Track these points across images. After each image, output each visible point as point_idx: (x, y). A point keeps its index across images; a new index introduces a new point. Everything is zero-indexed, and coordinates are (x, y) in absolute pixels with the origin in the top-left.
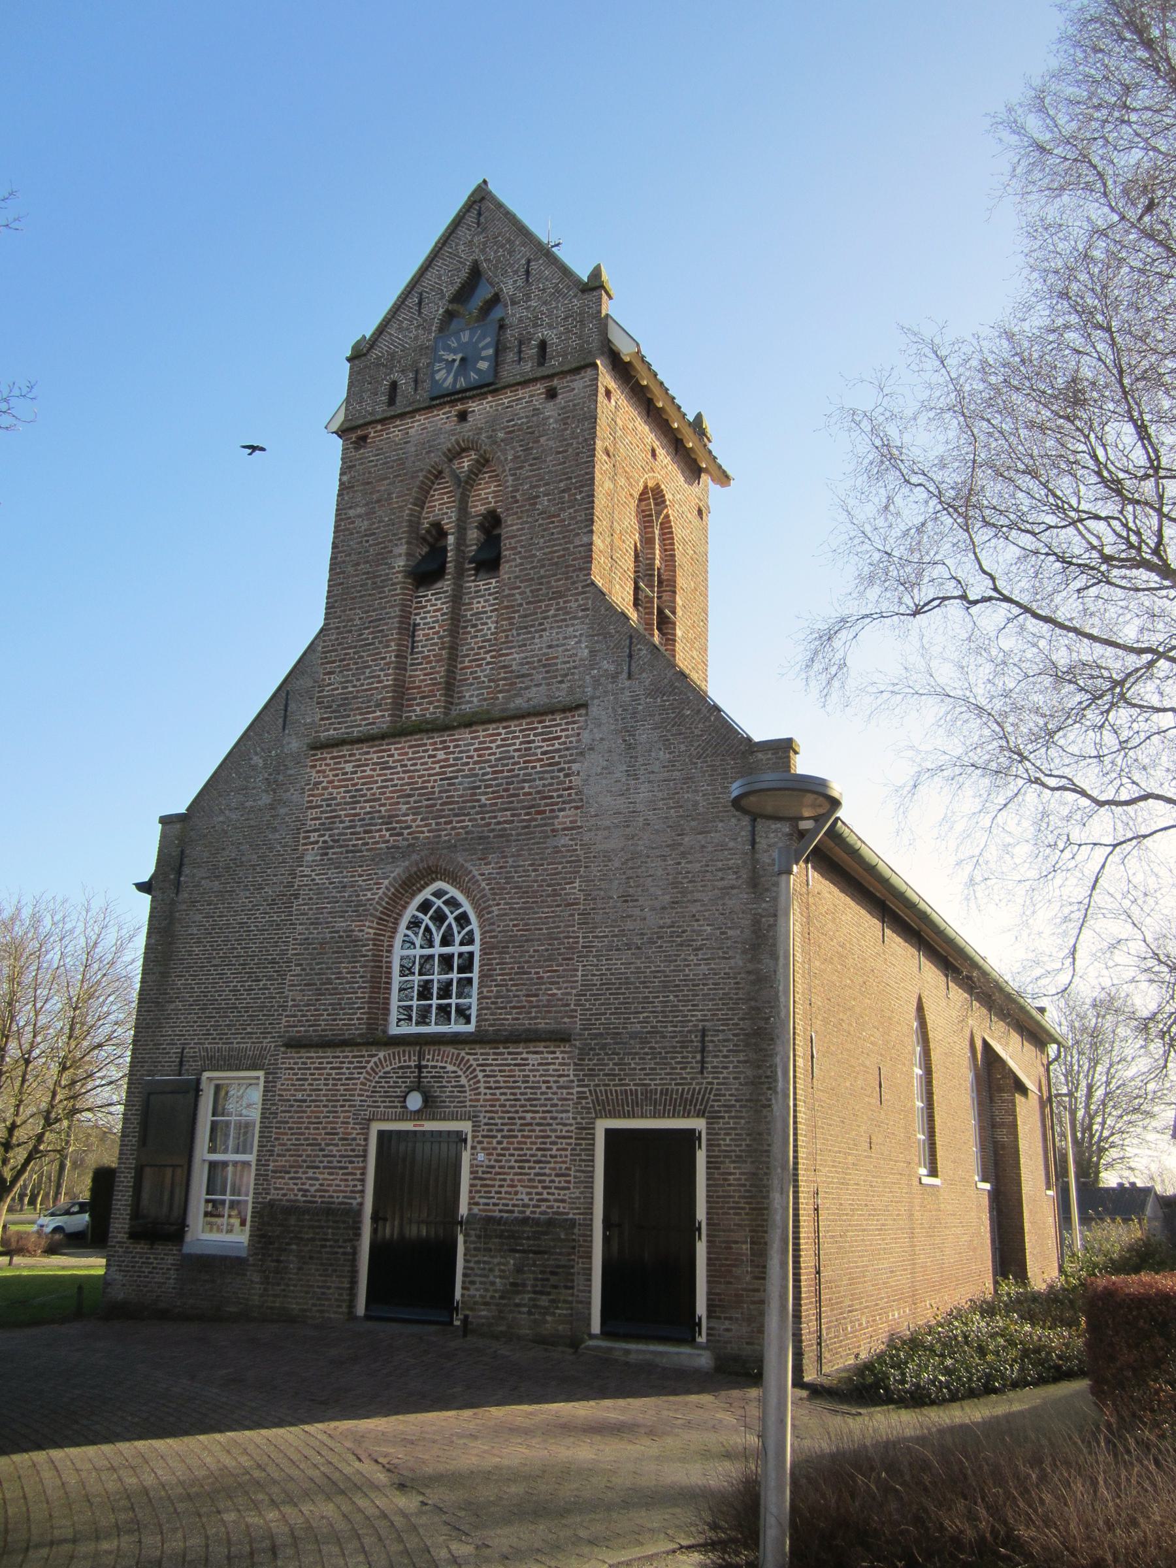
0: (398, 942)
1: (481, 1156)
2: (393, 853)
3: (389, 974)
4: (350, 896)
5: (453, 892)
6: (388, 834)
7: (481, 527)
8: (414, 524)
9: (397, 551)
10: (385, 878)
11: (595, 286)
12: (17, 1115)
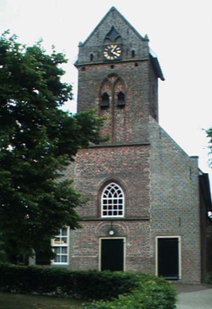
0: (102, 196)
1: (129, 244)
2: (102, 176)
3: (100, 204)
5: (116, 185)
7: (118, 96)
8: (100, 93)
9: (96, 100)
11: (146, 40)
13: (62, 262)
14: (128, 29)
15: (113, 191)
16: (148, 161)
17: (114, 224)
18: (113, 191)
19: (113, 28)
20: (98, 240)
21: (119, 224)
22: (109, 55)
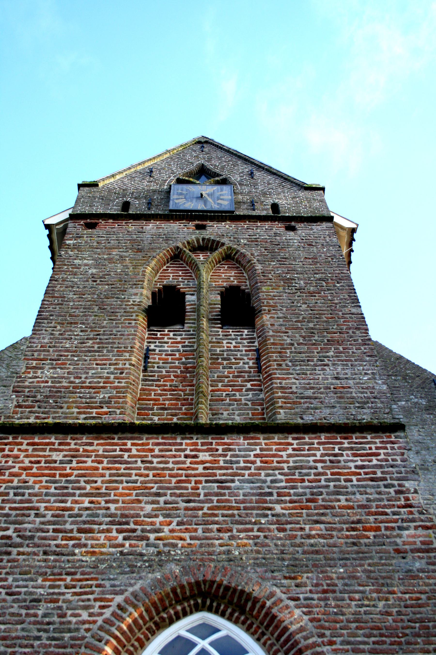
4: (45, 615)
6: (121, 537)
10: (116, 593)
12: (366, 546)
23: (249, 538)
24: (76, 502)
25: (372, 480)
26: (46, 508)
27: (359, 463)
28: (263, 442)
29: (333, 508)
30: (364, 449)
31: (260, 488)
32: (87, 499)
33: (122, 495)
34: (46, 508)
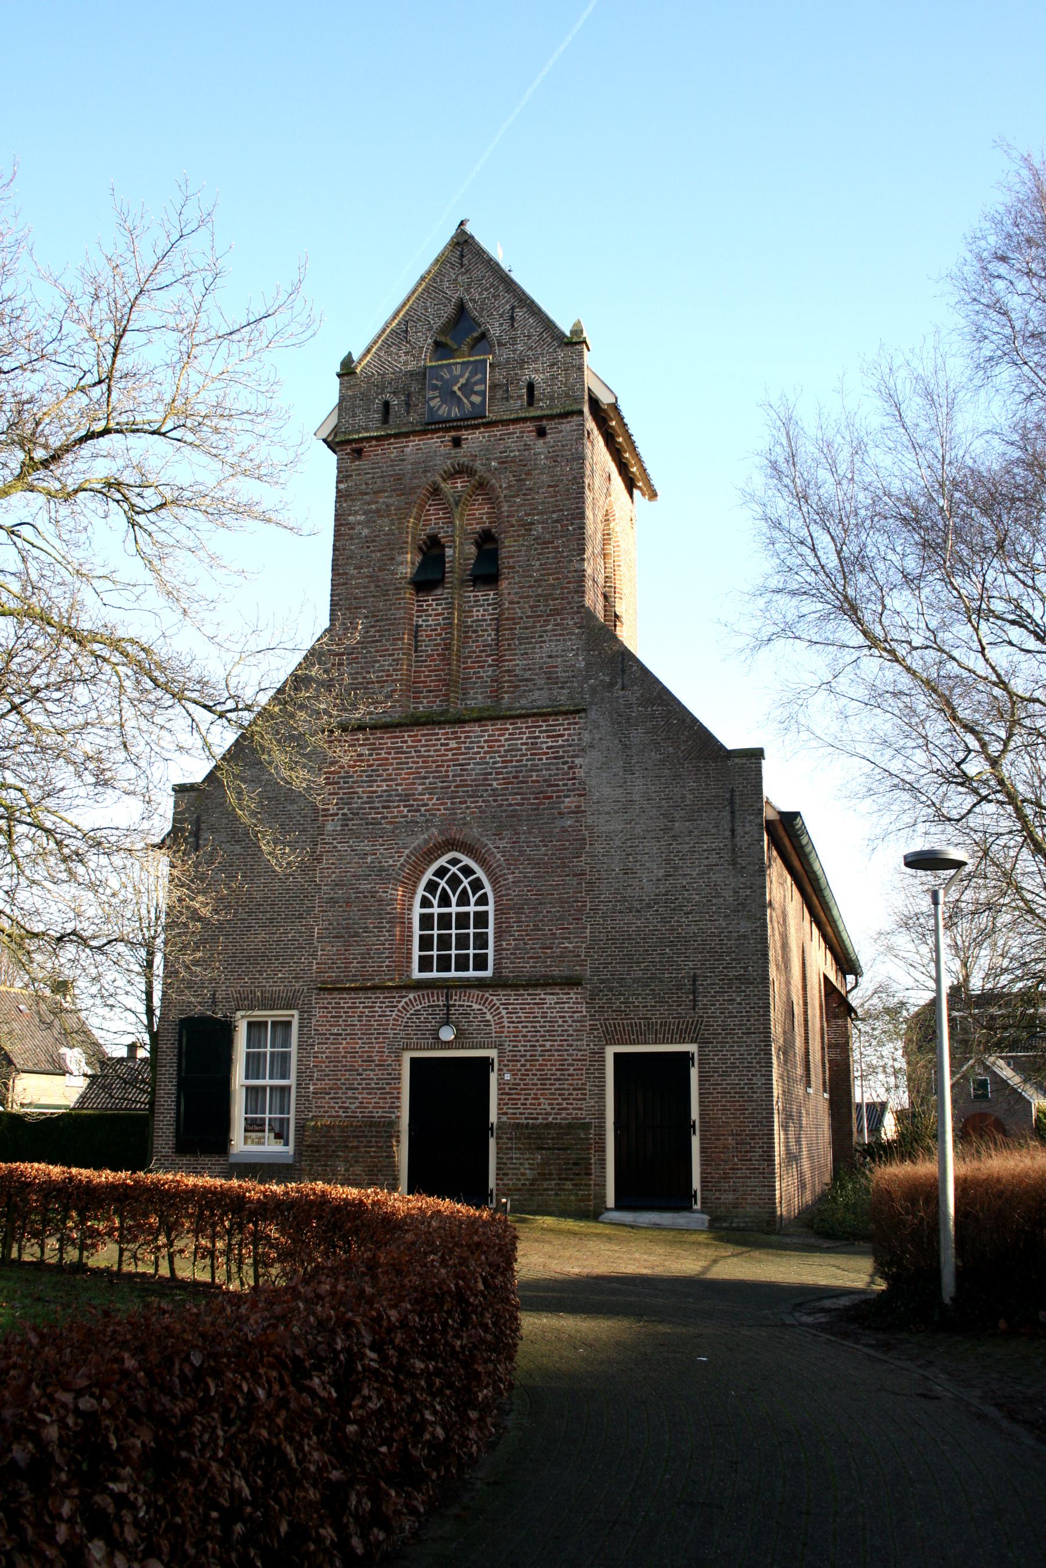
5: (467, 861)
11: (575, 342)
13: (271, 1078)
14: (513, 308)
15: (454, 882)
16: (581, 773)
17: (456, 1000)
18: (454, 882)
19: (461, 308)
20: (398, 1060)
21: (473, 1002)
22: (444, 402)
23: (476, 807)
24: (378, 786)
25: (555, 758)
26: (363, 792)
27: (550, 744)
28: (490, 728)
29: (527, 782)
30: (555, 731)
31: (486, 769)
32: (384, 784)
33: (404, 779)
34: (363, 792)
